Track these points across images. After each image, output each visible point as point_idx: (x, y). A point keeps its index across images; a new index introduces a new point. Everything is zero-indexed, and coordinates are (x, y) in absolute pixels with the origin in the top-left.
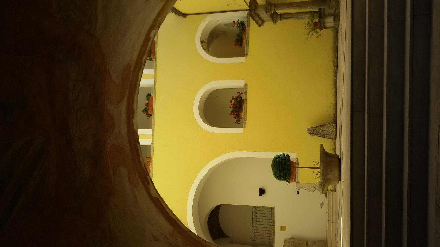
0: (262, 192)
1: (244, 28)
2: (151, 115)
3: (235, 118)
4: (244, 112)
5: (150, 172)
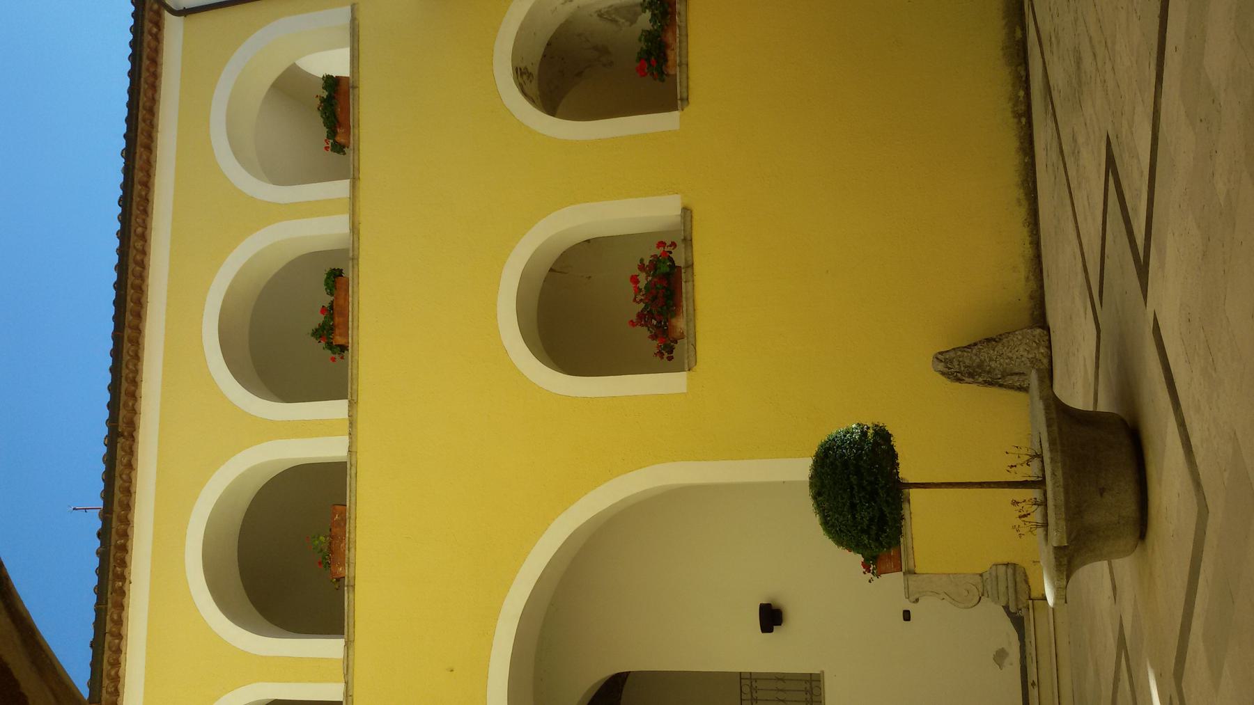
0: (771, 617)
1: (670, 10)
2: (343, 348)
3: (654, 337)
4: (685, 315)
5: (346, 559)
